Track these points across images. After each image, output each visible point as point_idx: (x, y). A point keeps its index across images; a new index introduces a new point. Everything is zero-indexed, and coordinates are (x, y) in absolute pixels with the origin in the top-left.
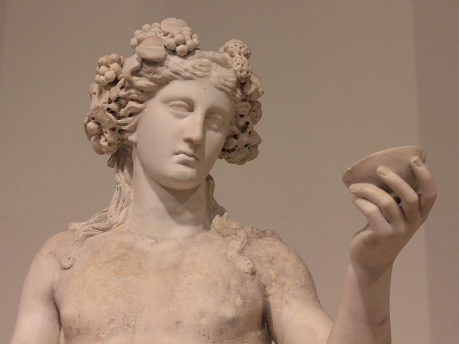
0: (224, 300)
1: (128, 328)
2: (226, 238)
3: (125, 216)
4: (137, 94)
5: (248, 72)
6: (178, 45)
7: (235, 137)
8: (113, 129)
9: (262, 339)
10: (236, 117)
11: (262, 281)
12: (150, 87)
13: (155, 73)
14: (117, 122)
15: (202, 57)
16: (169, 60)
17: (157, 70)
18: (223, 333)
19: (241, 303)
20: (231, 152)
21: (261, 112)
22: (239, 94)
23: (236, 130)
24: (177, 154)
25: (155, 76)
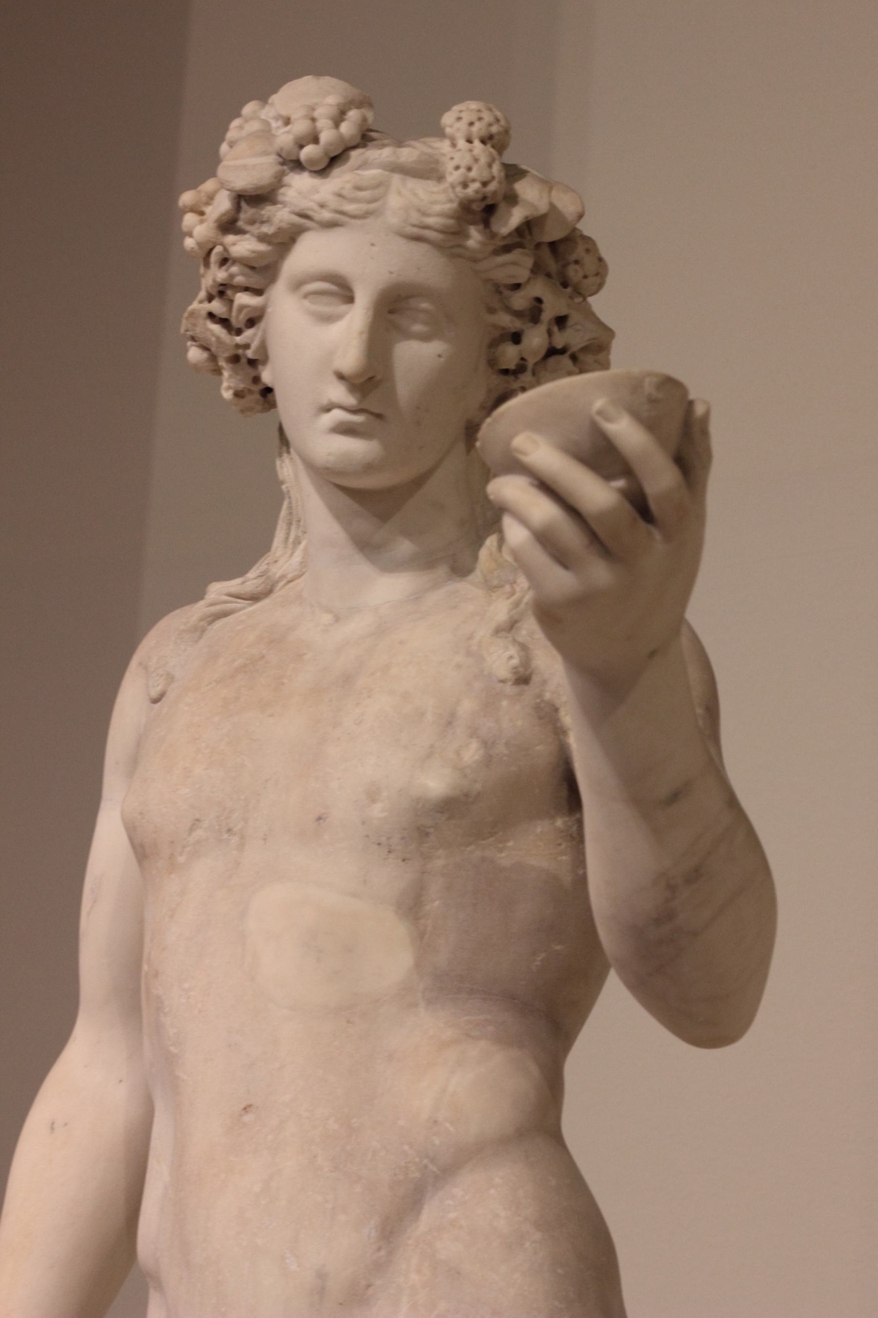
0: (430, 755)
1: (231, 837)
2: (494, 592)
3: (303, 558)
4: (243, 274)
5: (485, 184)
6: (301, 147)
7: (516, 338)
8: (235, 359)
9: (571, 836)
10: (500, 293)
11: (547, 696)
12: (260, 255)
13: (263, 222)
14: (234, 343)
15: (364, 165)
16: (289, 186)
17: (263, 215)
18: (427, 834)
19: (476, 757)
20: (520, 376)
21: (600, 260)
22: (475, 237)
23: (506, 320)
24: (328, 409)
25: (266, 229)
